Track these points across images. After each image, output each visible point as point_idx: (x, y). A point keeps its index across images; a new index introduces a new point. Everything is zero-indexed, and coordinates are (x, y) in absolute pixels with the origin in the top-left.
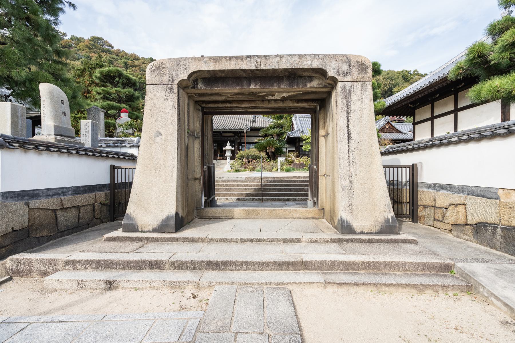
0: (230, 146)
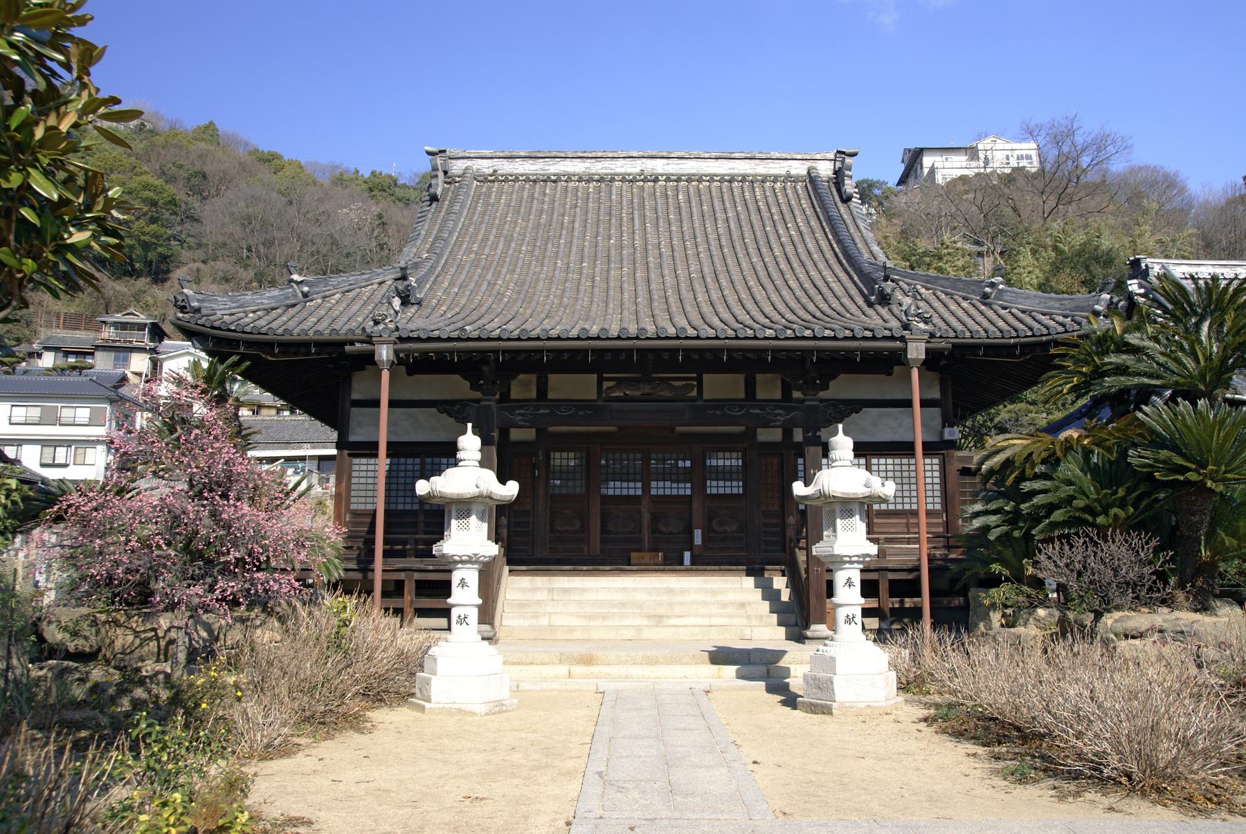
0: (483, 464)
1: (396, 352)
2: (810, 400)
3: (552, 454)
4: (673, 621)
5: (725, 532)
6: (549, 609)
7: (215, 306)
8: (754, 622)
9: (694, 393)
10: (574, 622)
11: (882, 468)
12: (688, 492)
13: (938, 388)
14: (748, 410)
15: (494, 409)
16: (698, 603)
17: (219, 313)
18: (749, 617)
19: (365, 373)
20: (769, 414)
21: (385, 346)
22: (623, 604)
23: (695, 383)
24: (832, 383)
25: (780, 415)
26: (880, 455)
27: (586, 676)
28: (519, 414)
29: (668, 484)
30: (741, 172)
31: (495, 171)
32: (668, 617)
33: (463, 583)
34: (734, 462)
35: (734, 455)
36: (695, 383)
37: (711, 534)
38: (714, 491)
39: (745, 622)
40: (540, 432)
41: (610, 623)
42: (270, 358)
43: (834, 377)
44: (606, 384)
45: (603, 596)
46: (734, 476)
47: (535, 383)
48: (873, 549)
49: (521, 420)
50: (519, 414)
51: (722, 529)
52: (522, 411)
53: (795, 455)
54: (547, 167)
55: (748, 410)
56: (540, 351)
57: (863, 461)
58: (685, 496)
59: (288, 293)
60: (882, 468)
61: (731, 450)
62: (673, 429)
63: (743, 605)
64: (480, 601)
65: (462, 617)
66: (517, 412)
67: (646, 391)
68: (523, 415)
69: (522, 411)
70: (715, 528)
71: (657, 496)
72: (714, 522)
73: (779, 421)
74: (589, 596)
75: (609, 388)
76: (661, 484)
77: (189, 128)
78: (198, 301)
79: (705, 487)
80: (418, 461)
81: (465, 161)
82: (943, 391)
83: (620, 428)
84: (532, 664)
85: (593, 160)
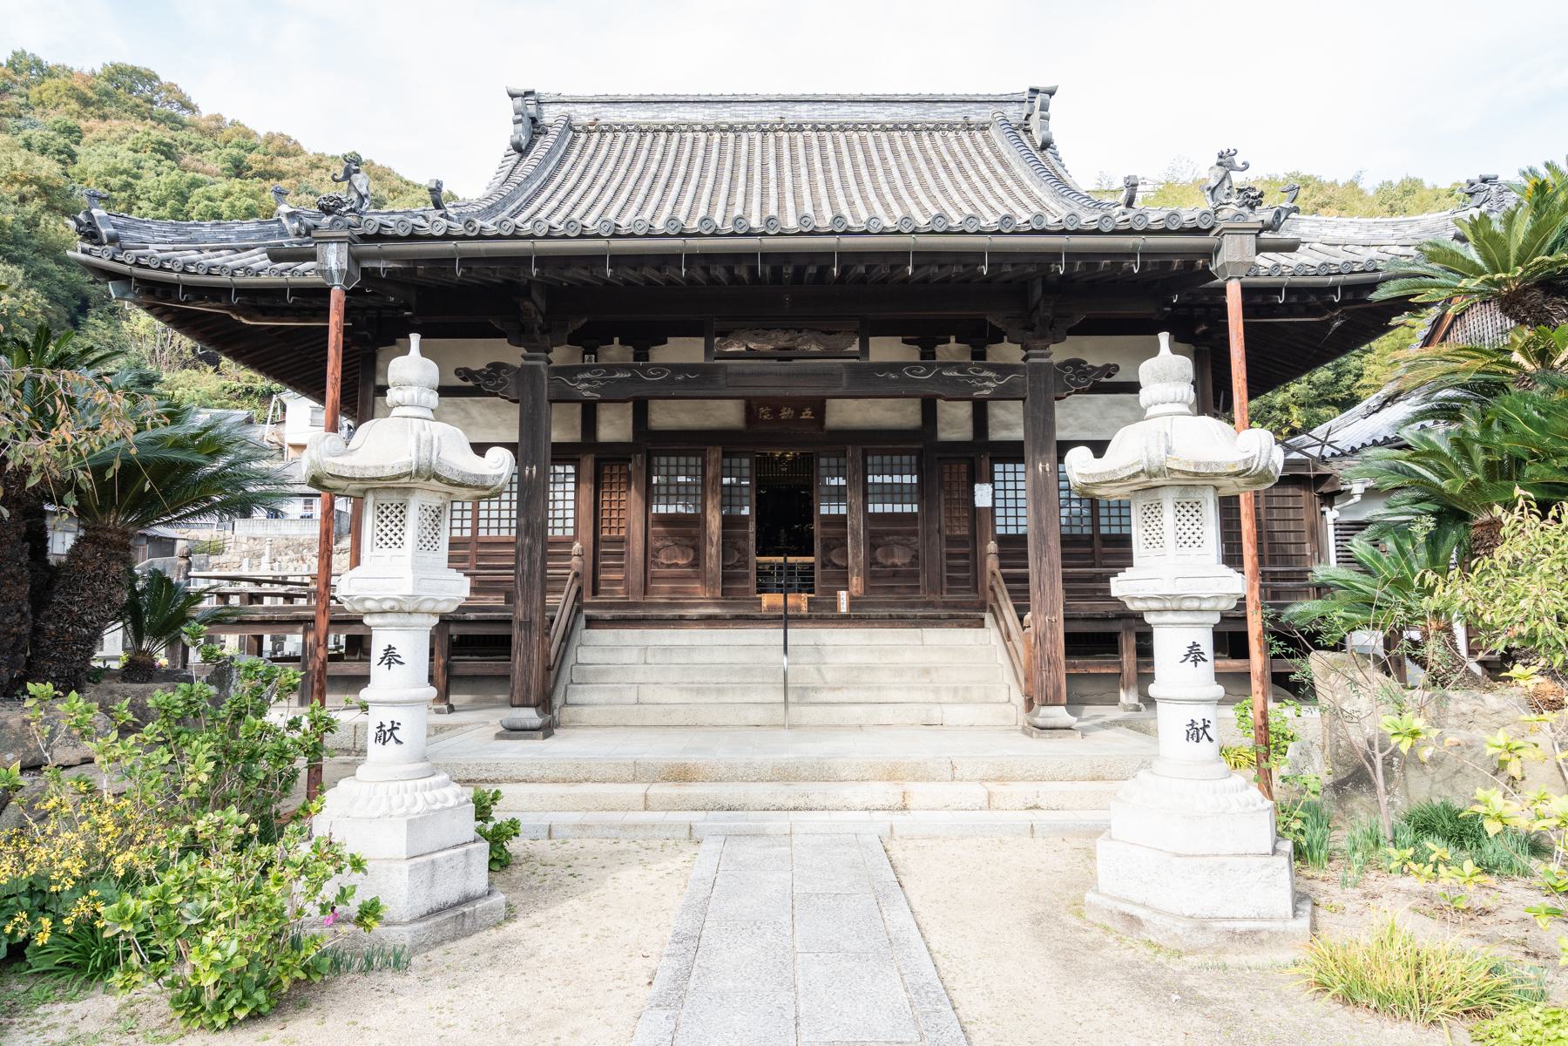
1: (355, 258)
2: (1036, 356)
3: (656, 459)
5: (894, 565)
6: (639, 678)
7: (146, 237)
8: (945, 697)
10: (675, 697)
14: (939, 373)
15: (545, 372)
16: (859, 669)
18: (937, 690)
20: (971, 378)
21: (334, 246)
22: (747, 670)
25: (990, 379)
27: (671, 806)
28: (583, 381)
30: (908, 119)
32: (816, 689)
33: (390, 656)
37: (874, 568)
39: (931, 697)
41: (727, 698)
42: (244, 321)
45: (720, 657)
49: (585, 390)
50: (583, 381)
51: (890, 562)
52: (587, 375)
53: (991, 459)
54: (663, 115)
55: (939, 373)
58: (838, 516)
59: (271, 229)
62: (819, 407)
63: (926, 671)
65: (389, 726)
66: (580, 377)
67: (781, 343)
68: (588, 381)
69: (587, 375)
70: (880, 559)
81: (559, 106)
84: (587, 780)
85: (720, 105)
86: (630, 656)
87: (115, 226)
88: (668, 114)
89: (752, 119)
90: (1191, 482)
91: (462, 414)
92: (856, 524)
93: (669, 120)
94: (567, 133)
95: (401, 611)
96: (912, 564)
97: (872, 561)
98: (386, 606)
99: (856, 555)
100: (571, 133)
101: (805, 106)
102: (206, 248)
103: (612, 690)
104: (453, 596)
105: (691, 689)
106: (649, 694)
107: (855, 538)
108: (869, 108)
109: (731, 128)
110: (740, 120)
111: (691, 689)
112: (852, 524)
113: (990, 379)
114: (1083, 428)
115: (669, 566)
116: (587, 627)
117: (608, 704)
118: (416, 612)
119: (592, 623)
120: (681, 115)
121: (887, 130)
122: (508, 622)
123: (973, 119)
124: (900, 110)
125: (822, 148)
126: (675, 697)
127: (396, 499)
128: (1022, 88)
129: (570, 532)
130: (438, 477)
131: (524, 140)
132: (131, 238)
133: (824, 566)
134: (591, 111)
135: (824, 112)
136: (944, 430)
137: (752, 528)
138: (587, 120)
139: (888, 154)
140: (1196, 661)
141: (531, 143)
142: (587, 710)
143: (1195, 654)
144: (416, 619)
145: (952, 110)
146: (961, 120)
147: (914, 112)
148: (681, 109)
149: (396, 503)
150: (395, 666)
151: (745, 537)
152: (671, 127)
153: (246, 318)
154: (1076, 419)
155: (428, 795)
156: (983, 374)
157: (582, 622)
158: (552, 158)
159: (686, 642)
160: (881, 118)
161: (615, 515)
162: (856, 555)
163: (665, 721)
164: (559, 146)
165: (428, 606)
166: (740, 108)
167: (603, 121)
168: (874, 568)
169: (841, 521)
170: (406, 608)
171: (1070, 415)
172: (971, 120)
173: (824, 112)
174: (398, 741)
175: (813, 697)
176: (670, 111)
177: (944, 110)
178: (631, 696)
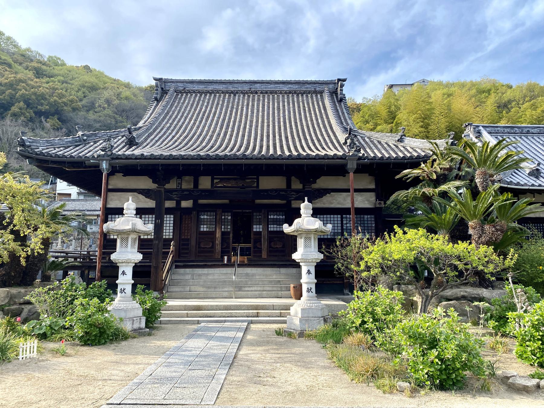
4: (247, 289)
5: (277, 248)
9: (255, 185)
11: (332, 219)
12: (261, 230)
13: (374, 184)
15: (163, 192)
17: (41, 148)
19: (115, 177)
20: (289, 194)
23: (256, 180)
24: (318, 181)
25: (294, 195)
26: (145, 214)
28: (175, 194)
29: (275, 226)
31: (185, 88)
33: (124, 273)
34: (272, 217)
35: (281, 213)
36: (256, 180)
37: (270, 249)
38: (272, 229)
40: (195, 203)
43: (319, 178)
44: (215, 181)
46: (205, 223)
47: (193, 181)
48: (321, 256)
49: (175, 197)
50: (175, 194)
51: (276, 246)
54: (208, 87)
56: (178, 165)
57: (138, 216)
60: (332, 219)
61: (280, 211)
64: (133, 282)
66: (174, 193)
69: (176, 193)
70: (273, 246)
71: (256, 232)
72: (272, 243)
73: (293, 197)
74: (210, 277)
75: (216, 183)
76: (258, 226)
77: (144, 87)
78: (30, 142)
79: (268, 228)
80: (339, 216)
82: (376, 185)
83: (230, 201)
86: (188, 277)
87: (30, 142)
88: (210, 87)
89: (240, 89)
90: (308, 232)
91: (136, 198)
92: (265, 235)
93: (210, 89)
94: (174, 94)
95: (127, 262)
96: (282, 247)
97: (270, 246)
98: (123, 261)
99: (264, 245)
100: (175, 93)
101: (258, 85)
102: (56, 147)
103: (182, 287)
104: (138, 259)
105: (206, 287)
106: (193, 288)
107: (264, 239)
108: (281, 85)
109: (232, 92)
110: (236, 89)
111: (206, 287)
112: (263, 234)
113: (294, 195)
114: (338, 204)
115: (204, 248)
116: (175, 268)
117: (180, 292)
118: (130, 262)
119: (177, 267)
120: (215, 87)
121: (287, 93)
122: (150, 266)
123: (318, 89)
124: (292, 86)
125: (264, 101)
126: (201, 289)
127: (126, 236)
128: (335, 78)
129: (171, 237)
130: (136, 232)
131: (158, 97)
132: (34, 145)
133: (254, 248)
134: (183, 85)
135: (265, 87)
136: (293, 204)
137: (231, 235)
138: (182, 89)
139: (286, 104)
140: (309, 274)
141: (162, 96)
142: (174, 294)
143: (309, 272)
144: (130, 264)
145: (310, 86)
146: (313, 90)
147: (297, 87)
148: (215, 85)
149: (126, 237)
150: (125, 275)
151: (229, 238)
152: (211, 91)
153: (68, 168)
154: (336, 201)
155: (132, 305)
156: (292, 193)
157: (174, 267)
158: (168, 105)
159: (206, 272)
160: (285, 89)
161: (186, 231)
162: (264, 245)
163: (198, 297)
164: (171, 99)
165: (133, 261)
166: (235, 85)
167: (187, 89)
168: (270, 249)
169: (259, 233)
170: (128, 261)
171: (334, 199)
172: (317, 90)
173: (265, 87)
174: (125, 293)
175: (243, 289)
176: (211, 86)
177: (308, 86)
178: (188, 289)
